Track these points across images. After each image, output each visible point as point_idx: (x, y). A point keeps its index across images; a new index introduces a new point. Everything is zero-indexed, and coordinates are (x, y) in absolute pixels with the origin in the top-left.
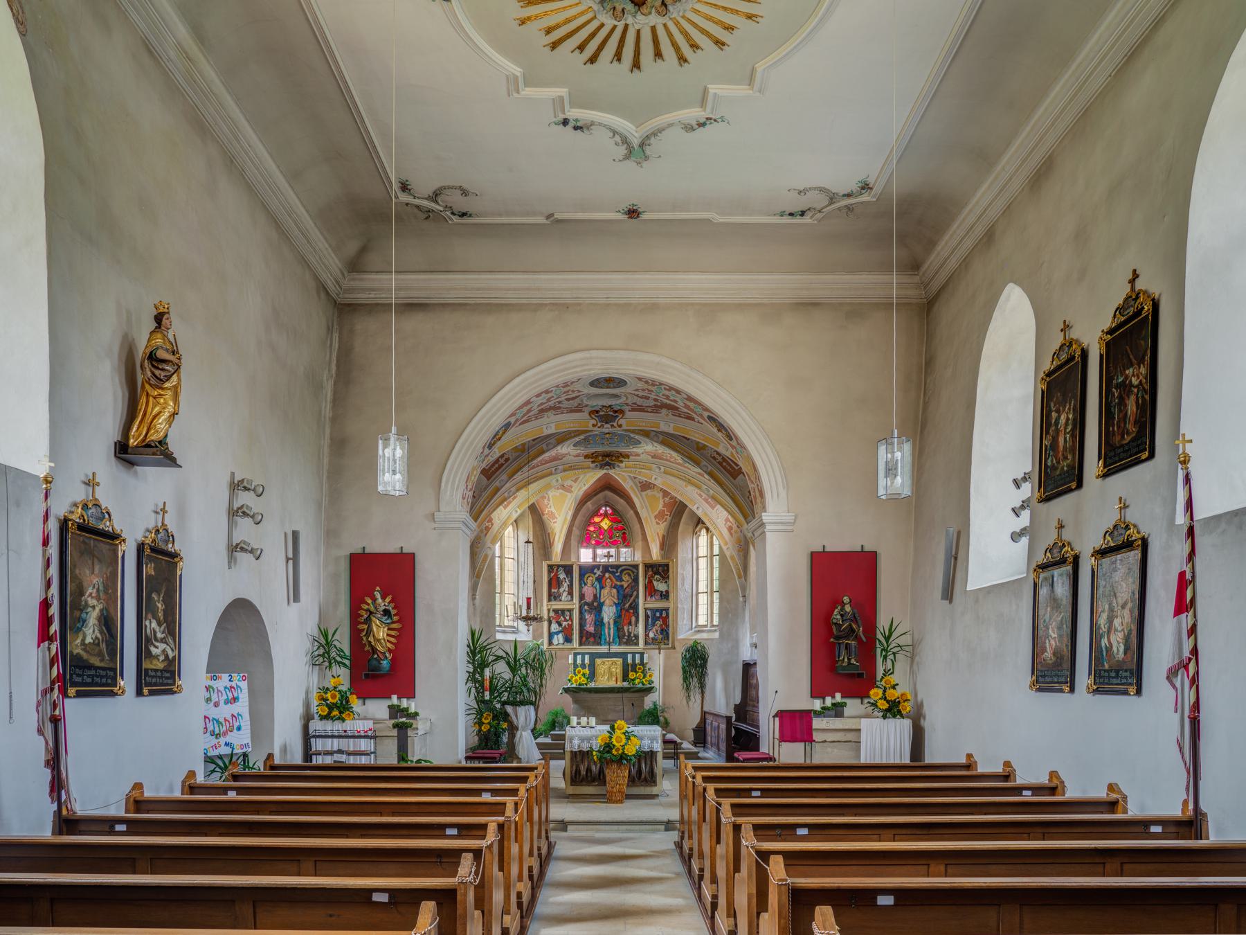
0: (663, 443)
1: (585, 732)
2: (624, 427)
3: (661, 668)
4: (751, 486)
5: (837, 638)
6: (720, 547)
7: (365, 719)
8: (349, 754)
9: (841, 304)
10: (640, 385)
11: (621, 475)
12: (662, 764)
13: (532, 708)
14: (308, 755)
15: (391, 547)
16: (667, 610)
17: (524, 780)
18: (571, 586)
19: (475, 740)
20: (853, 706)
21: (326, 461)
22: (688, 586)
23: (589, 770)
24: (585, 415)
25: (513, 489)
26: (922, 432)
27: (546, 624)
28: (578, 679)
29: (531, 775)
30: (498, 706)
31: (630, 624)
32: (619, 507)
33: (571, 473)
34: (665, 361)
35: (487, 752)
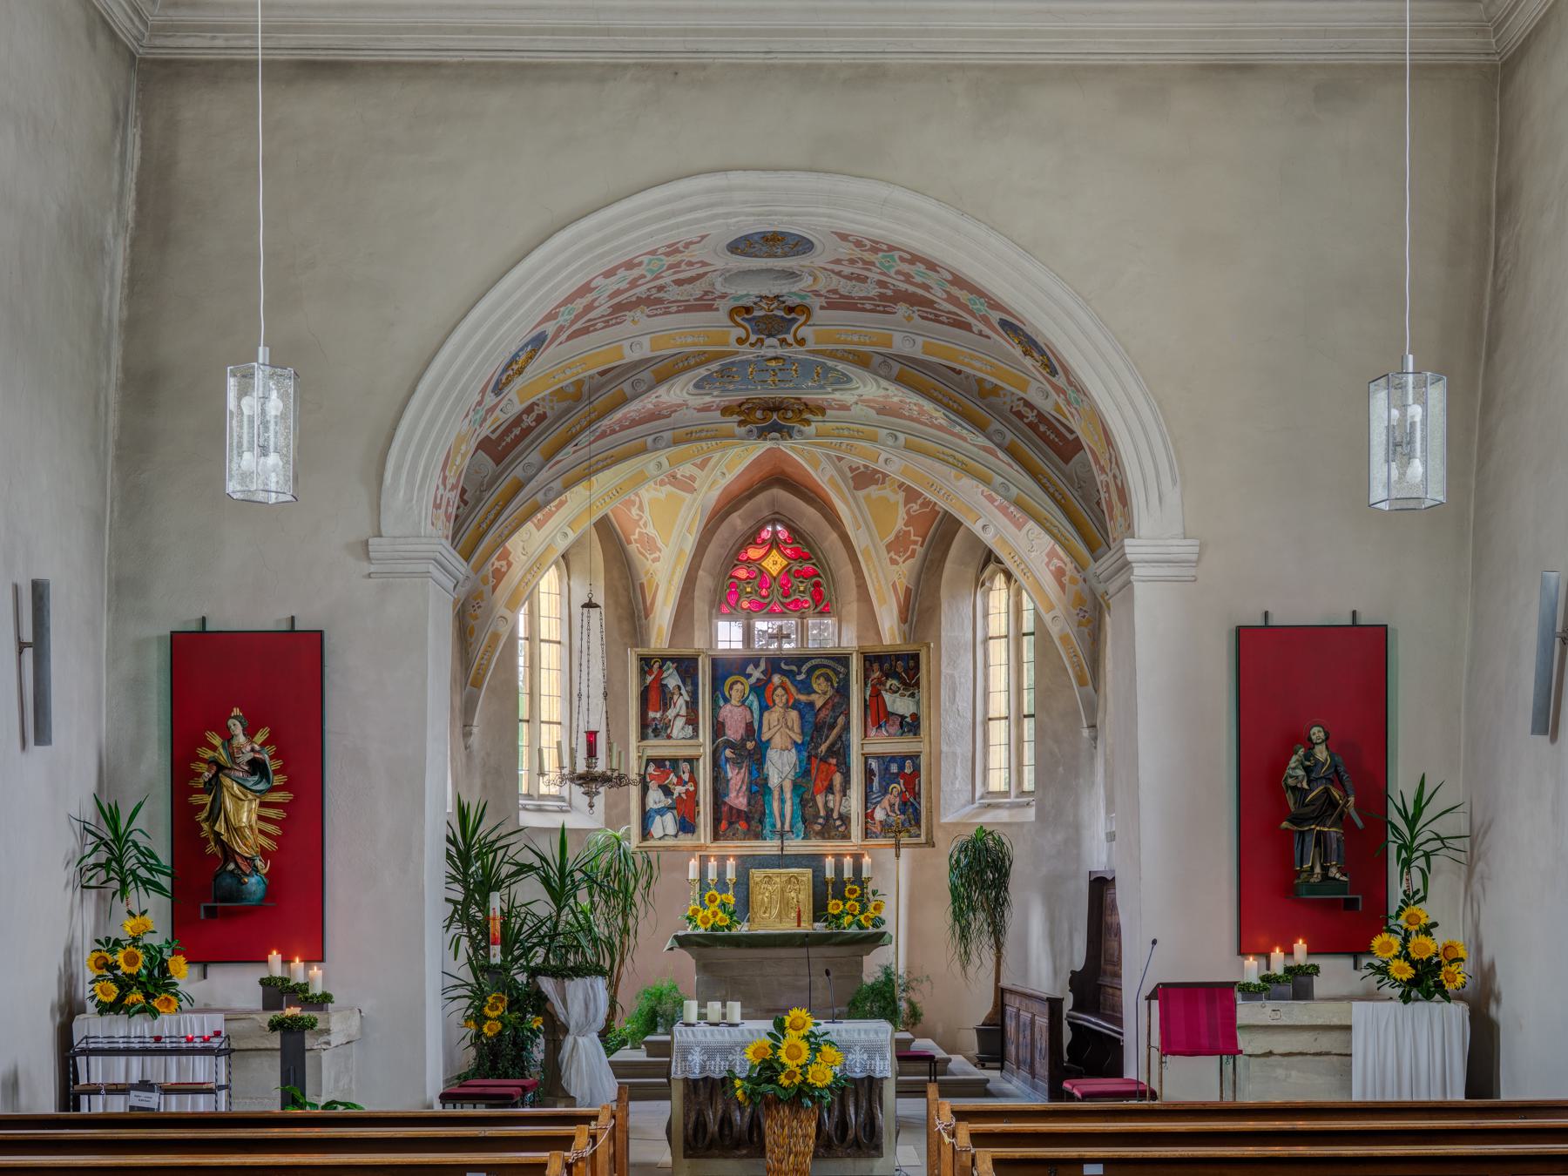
0: (900, 380)
1: (719, 1036)
2: (810, 345)
3: (904, 890)
4: (1100, 478)
5: (1297, 820)
6: (1038, 618)
7: (207, 1010)
8: (167, 1091)
9: (1304, 68)
10: (846, 251)
11: (803, 452)
12: (894, 1107)
13: (600, 984)
14: (69, 1092)
15: (268, 617)
16: (915, 757)
17: (566, 1142)
18: (693, 705)
19: (467, 1057)
20: (1335, 973)
21: (113, 420)
22: (964, 704)
23: (726, 1121)
24: (721, 316)
25: (557, 485)
26: (1489, 356)
27: (635, 792)
28: (709, 917)
29: (581, 1133)
30: (522, 978)
31: (830, 789)
32: (804, 525)
33: (694, 447)
34: (899, 195)
35: (494, 1085)
